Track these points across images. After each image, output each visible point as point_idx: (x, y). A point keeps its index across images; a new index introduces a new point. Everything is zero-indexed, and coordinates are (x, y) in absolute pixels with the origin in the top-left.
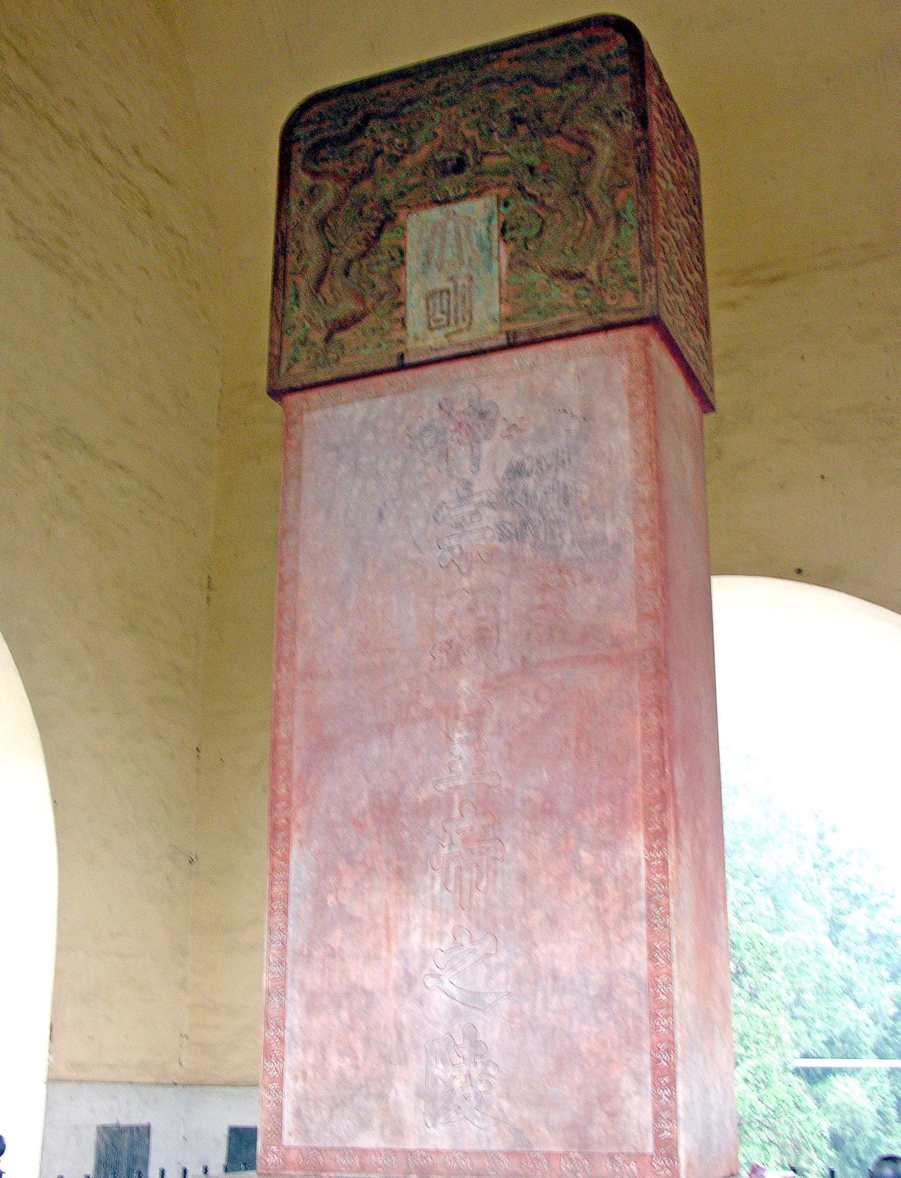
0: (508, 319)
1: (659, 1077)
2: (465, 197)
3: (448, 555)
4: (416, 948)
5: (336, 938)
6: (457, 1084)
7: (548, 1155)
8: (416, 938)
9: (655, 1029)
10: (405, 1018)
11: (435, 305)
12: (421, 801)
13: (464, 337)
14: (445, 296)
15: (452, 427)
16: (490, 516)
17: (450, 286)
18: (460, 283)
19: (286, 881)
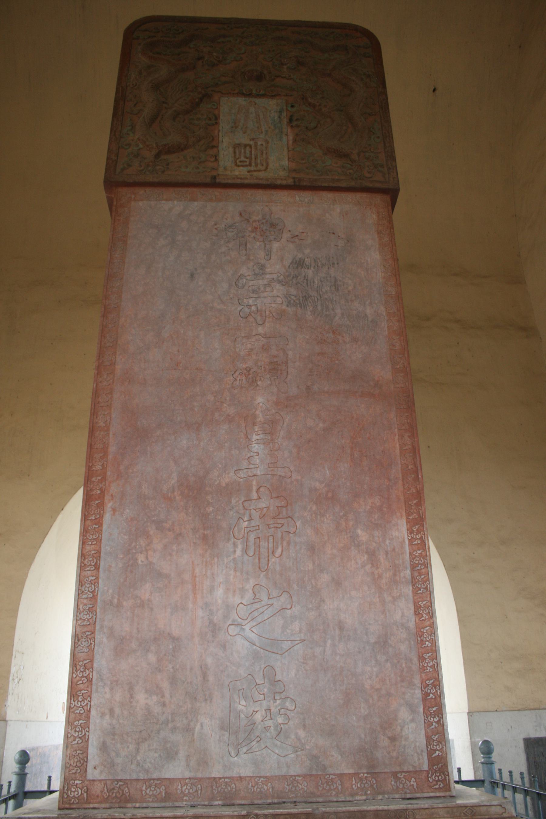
3: (247, 310)
4: (220, 601)
6: (258, 717)
7: (341, 776)
8: (220, 592)
11: (240, 152)
12: (224, 485)
13: (262, 175)
14: (248, 148)
16: (279, 290)
17: (252, 143)
18: (259, 143)
19: (99, 541)
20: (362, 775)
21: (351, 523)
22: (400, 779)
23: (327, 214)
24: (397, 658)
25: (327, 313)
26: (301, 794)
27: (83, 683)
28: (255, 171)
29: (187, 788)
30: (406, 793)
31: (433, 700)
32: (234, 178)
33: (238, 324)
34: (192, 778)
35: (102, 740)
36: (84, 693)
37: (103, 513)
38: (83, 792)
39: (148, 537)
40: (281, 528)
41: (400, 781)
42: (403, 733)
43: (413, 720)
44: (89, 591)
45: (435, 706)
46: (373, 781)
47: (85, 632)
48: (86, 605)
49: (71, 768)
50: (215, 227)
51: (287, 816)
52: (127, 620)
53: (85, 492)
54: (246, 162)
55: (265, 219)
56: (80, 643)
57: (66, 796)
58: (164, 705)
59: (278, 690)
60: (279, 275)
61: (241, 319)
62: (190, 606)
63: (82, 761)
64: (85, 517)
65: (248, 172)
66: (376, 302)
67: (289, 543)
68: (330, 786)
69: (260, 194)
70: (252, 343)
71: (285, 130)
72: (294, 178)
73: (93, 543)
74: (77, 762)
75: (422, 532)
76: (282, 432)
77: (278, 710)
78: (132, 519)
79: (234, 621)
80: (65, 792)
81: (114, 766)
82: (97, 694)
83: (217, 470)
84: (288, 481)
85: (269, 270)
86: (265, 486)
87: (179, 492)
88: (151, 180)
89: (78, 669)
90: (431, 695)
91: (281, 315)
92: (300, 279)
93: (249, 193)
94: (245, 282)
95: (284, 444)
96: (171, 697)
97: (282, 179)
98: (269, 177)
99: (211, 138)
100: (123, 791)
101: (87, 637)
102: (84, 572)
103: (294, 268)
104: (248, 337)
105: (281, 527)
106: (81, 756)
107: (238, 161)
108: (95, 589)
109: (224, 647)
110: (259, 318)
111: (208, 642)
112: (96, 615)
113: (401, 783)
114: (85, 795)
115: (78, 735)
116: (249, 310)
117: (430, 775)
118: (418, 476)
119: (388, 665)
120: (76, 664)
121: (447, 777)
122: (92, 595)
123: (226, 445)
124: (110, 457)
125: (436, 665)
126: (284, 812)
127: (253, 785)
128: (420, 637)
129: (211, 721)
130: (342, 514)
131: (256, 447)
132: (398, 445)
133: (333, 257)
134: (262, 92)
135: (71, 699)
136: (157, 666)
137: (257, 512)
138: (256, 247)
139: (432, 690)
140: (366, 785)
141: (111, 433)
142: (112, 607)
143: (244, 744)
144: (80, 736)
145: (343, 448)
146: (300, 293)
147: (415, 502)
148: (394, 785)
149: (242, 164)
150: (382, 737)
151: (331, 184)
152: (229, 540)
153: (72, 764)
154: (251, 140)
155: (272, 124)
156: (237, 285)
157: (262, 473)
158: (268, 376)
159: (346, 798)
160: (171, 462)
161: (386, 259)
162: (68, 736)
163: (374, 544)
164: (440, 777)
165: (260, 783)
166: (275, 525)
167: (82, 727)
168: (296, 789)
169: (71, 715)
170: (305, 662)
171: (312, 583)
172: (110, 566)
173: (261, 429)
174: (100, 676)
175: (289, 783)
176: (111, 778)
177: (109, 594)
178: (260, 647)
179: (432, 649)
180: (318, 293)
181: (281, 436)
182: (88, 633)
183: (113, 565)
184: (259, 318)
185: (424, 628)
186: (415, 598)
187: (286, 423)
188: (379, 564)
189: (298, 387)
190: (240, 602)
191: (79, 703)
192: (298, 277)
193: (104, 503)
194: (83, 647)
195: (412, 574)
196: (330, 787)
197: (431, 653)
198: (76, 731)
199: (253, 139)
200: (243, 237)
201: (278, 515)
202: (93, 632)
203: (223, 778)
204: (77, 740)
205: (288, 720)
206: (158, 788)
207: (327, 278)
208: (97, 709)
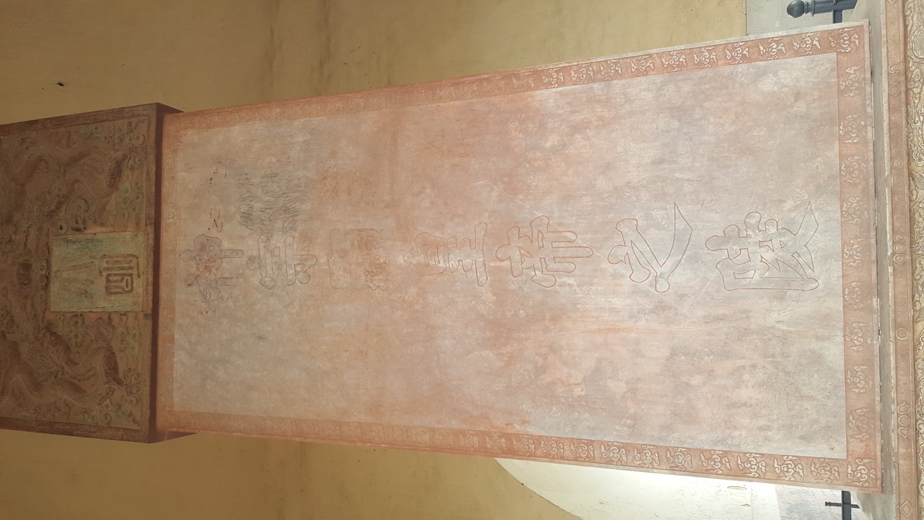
0: (137, 224)
1: (760, 54)
2: (48, 262)
3: (300, 276)
4: (628, 301)
5: (617, 387)
6: (769, 256)
7: (841, 157)
8: (618, 302)
9: (713, 63)
10: (700, 313)
11: (116, 287)
12: (494, 298)
13: (142, 262)
14: (111, 278)
15: (207, 274)
16: (278, 240)
17: (105, 274)
18: (105, 265)
19: (558, 440)
20: (841, 132)
21: (538, 154)
22: (848, 86)
23: (189, 187)
24: (699, 95)
25: (303, 185)
26: (864, 204)
27: (728, 462)
28: (138, 269)
29: (857, 340)
30: (864, 79)
31: (751, 50)
32: (147, 293)
33: (316, 285)
34: (844, 333)
35: (798, 441)
36: (741, 460)
37: (527, 435)
38: (862, 463)
39: (554, 384)
40: (544, 234)
41: (849, 86)
42: (791, 84)
43: (775, 74)
44: (618, 453)
45: (759, 47)
46: (849, 118)
47: (668, 459)
48: (634, 457)
49: (832, 477)
50: (204, 313)
51: (895, 217)
52: (651, 408)
53: (504, 455)
54: (127, 280)
55: (195, 257)
56: (680, 465)
57: (867, 484)
58: (754, 366)
59: (736, 233)
60: (260, 240)
61: (311, 282)
62: (633, 335)
63: (824, 464)
64: (530, 456)
65: (139, 277)
66: (289, 130)
67: (561, 224)
68: (854, 170)
69: (165, 264)
70: (338, 269)
71: (89, 237)
72: (146, 225)
73: (562, 446)
74: (825, 471)
75: (550, 71)
76: (436, 234)
77: (760, 233)
78: (534, 402)
79: (651, 285)
80: (862, 484)
81: (829, 427)
82: (742, 446)
83: (479, 305)
84: (490, 226)
85: (255, 252)
86: (496, 252)
87: (503, 348)
88: (148, 389)
89: (712, 468)
90: (745, 52)
91: (306, 238)
92: (264, 217)
93: (164, 275)
94: (268, 279)
95: (449, 232)
96: (744, 358)
97: (148, 239)
98: (145, 253)
99: (100, 320)
100: (860, 416)
101: (672, 457)
102: (596, 458)
103: (252, 224)
104: (331, 274)
105: (542, 233)
106: (818, 466)
107: (127, 289)
108: (615, 446)
109: (682, 296)
110: (310, 263)
111: (676, 314)
112: (646, 445)
113: (852, 85)
114: (865, 461)
115: (793, 469)
116: (300, 273)
117: (843, 51)
118: (485, 79)
119: (706, 104)
120: (706, 470)
121: (845, 30)
122: (623, 450)
123: (450, 296)
124: (464, 427)
125: (709, 48)
126: (889, 220)
127: (853, 260)
128: (674, 68)
129: (773, 311)
130: (528, 165)
131: (453, 263)
132: (451, 103)
133: (239, 180)
134: (44, 264)
135: (749, 477)
136: (706, 374)
137: (525, 260)
138: (228, 267)
139: (739, 52)
140: (854, 126)
141: (437, 426)
142: (636, 427)
143: (801, 272)
144: (793, 466)
145: (453, 166)
146: (281, 216)
147: (515, 81)
148: (854, 93)
149: (130, 285)
150: (795, 108)
151: (153, 181)
152: (557, 292)
153: (828, 476)
154: (101, 275)
155: (82, 251)
156: (272, 287)
157: (482, 256)
158: (374, 251)
159: (870, 150)
160: (469, 357)
161: (240, 119)
162: (793, 481)
163: (563, 126)
164: (846, 38)
165: (851, 253)
166: (540, 240)
167: (783, 464)
168: (858, 210)
169: (768, 477)
170: (701, 202)
171: (607, 197)
172: (589, 427)
173: (433, 257)
174: (720, 441)
175: (851, 218)
176: (845, 430)
177: (621, 429)
178: (683, 255)
179: (689, 54)
180: (280, 197)
181: (441, 235)
182: (668, 455)
183: (587, 424)
184: (310, 263)
185: (663, 64)
186: (626, 76)
187: (427, 230)
188: (585, 120)
189: (386, 217)
190: (629, 278)
191: (753, 467)
192: (262, 219)
193: (516, 434)
194: (685, 461)
195: (599, 81)
196: (856, 169)
197: (693, 55)
198: (787, 472)
199: (101, 272)
200: (217, 282)
201: (529, 237)
202: (667, 449)
203: (844, 297)
204: (798, 470)
205: (314, 258)
206: (856, 374)
207: (262, 186)
208: (760, 446)
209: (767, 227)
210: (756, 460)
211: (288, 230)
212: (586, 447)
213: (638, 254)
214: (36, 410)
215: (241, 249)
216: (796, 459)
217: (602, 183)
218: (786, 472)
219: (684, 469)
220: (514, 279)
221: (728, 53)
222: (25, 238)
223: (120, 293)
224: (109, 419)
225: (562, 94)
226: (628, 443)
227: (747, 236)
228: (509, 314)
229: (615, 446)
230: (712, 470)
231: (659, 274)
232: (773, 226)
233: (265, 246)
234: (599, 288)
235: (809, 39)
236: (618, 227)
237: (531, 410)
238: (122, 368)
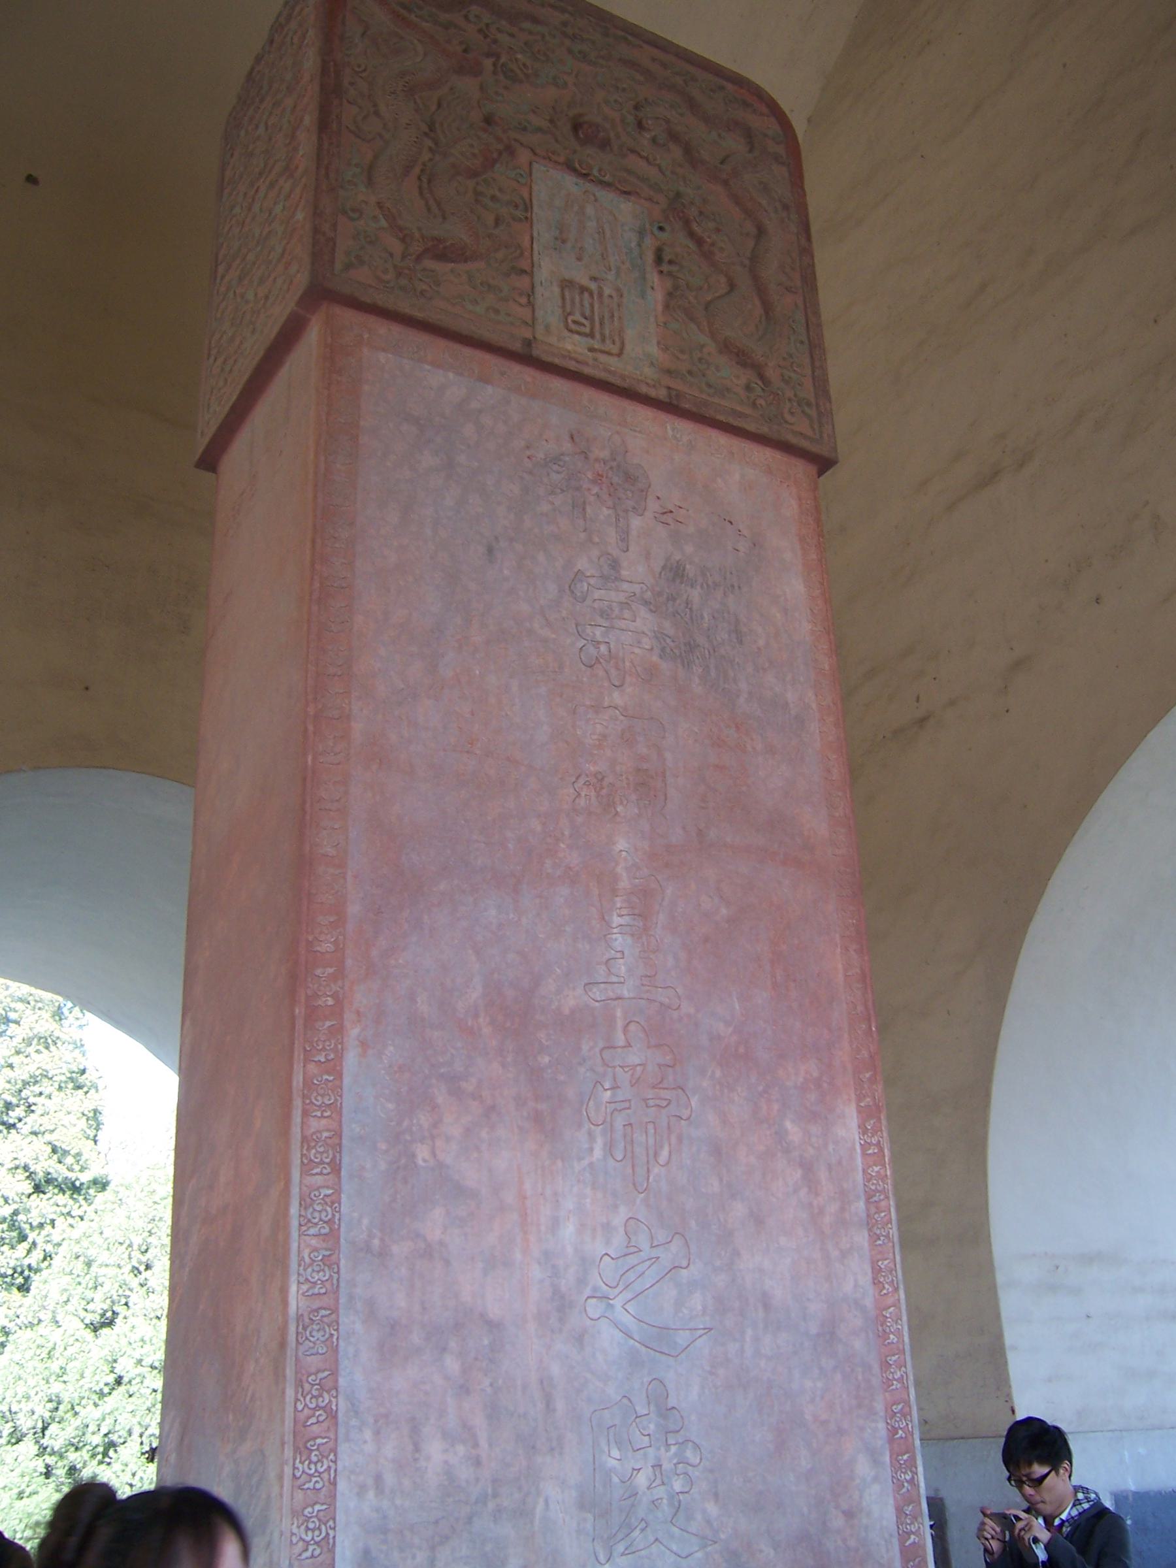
0: (669, 372)
4: (570, 1250)
6: (642, 1480)
8: (569, 1230)
10: (556, 1370)
14: (586, 295)
15: (590, 475)
16: (645, 620)
17: (593, 286)
21: (776, 1107)
27: (318, 1422)
32: (564, 357)
33: (577, 677)
43: (876, 1479)
44: (321, 1220)
47: (317, 1310)
48: (316, 1250)
50: (528, 453)
56: (308, 1333)
58: (477, 1462)
59: (672, 1427)
62: (518, 1256)
67: (680, 1139)
69: (605, 402)
73: (326, 1114)
84: (675, 1014)
92: (680, 605)
93: (588, 394)
94: (586, 589)
108: (333, 1215)
110: (613, 672)
112: (338, 1273)
128: (882, 1326)
131: (619, 941)
143: (620, 1536)
151: (731, 420)
152: (580, 1126)
163: (811, 1151)
167: (319, 1520)
169: (295, 1494)
171: (719, 1220)
172: (363, 1168)
174: (353, 1405)
178: (639, 1343)
182: (323, 1312)
183: (368, 1166)
184: (613, 672)
190: (604, 1253)
191: (313, 1466)
194: (314, 1343)
195: (868, 1210)
198: (307, 1529)
201: (660, 1083)
202: (335, 1310)
204: (311, 1548)
209: (682, 1476)
210: (325, 1470)
211: (661, 643)
212: (327, 1160)
213: (640, 1268)
214: (365, 70)
215: (630, 549)
216: (329, 1543)
217: (739, 1209)
218: (307, 1527)
219: (301, 1341)
220: (597, 1050)
221: (900, 1407)
222: (646, 155)
223: (563, 306)
224: (351, 214)
225: (853, 1149)
226: (339, 1238)
227: (668, 1445)
228: (542, 1036)
229: (333, 1215)
230: (303, 1392)
231: (611, 1302)
232: (683, 1486)
233: (635, 595)
234: (588, 1200)
235: (917, 1527)
236: (677, 1236)
237: (386, 1061)
238: (438, 266)
